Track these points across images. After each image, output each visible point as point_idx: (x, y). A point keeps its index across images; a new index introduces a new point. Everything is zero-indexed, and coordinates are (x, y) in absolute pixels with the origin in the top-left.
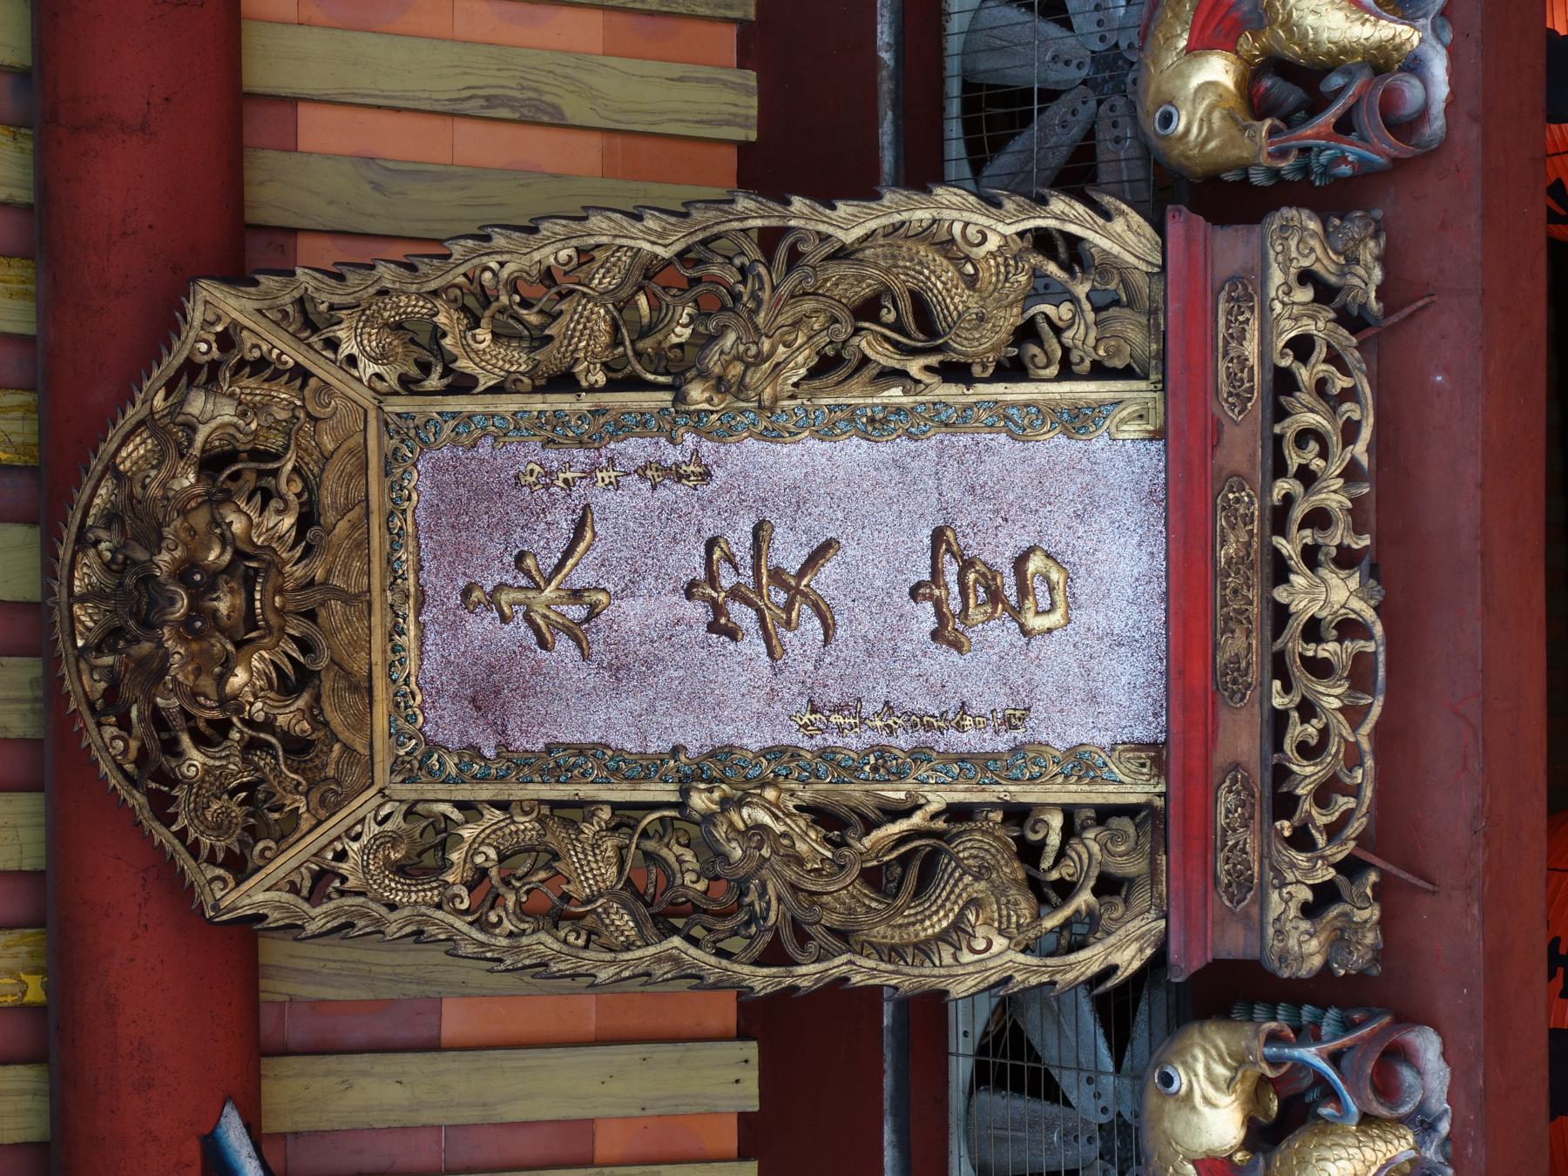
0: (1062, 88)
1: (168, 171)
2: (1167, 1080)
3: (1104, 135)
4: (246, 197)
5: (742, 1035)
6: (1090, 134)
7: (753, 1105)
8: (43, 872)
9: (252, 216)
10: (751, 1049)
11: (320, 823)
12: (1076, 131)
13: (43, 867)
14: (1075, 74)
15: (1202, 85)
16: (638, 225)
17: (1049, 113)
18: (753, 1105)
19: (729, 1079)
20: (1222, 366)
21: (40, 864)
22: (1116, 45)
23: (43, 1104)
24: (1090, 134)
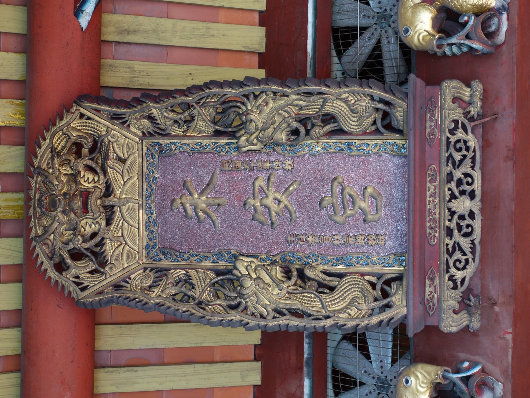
0: (367, 26)
1: (72, 80)
2: (407, 381)
3: (384, 41)
4: (95, 377)
5: (256, 359)
6: (379, 41)
7: (259, 383)
8: (21, 310)
9: (103, 38)
10: (258, 364)
11: (112, 130)
12: (374, 41)
13: (21, 308)
14: (372, 21)
15: (422, 24)
16: (445, 273)
17: (363, 35)
18: (259, 383)
19: (252, 375)
20: (428, 124)
21: (20, 307)
22: (386, 10)
23: (20, 379)
24: (379, 41)
